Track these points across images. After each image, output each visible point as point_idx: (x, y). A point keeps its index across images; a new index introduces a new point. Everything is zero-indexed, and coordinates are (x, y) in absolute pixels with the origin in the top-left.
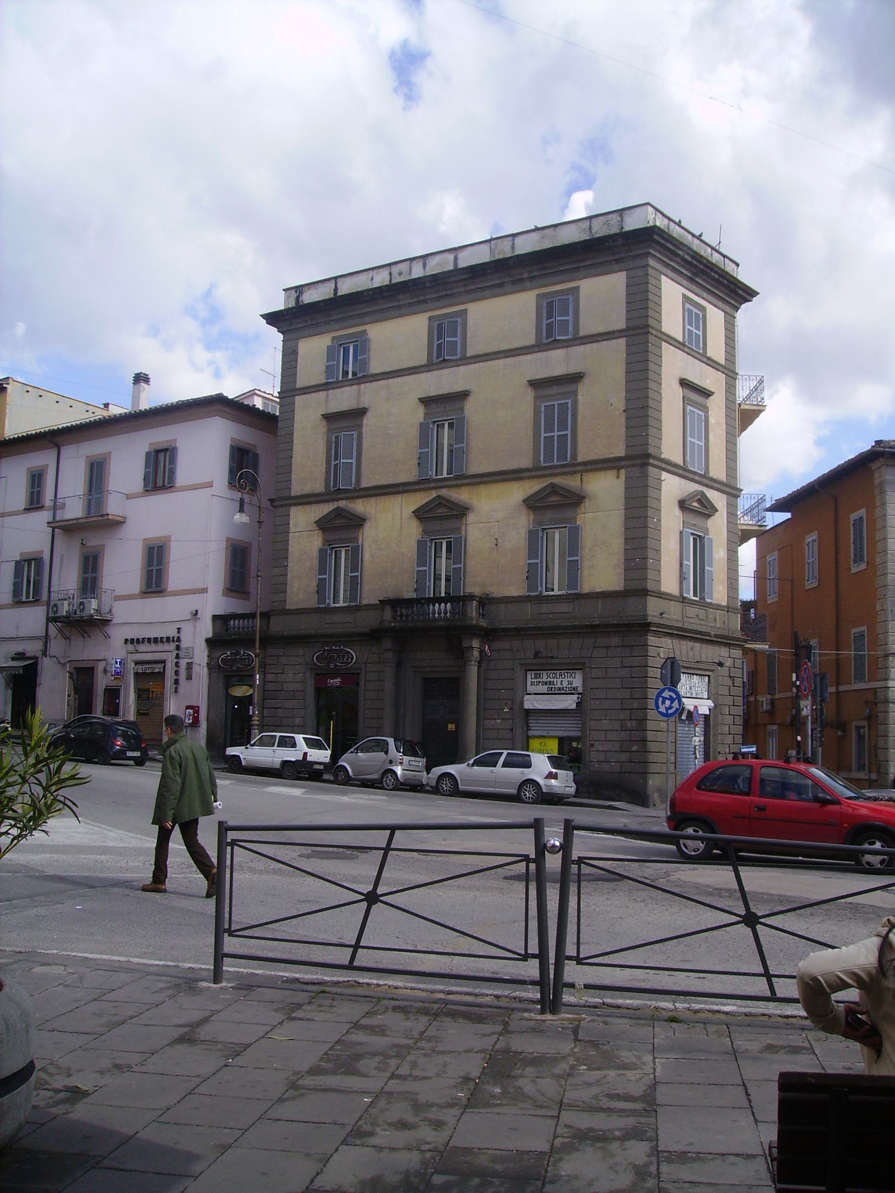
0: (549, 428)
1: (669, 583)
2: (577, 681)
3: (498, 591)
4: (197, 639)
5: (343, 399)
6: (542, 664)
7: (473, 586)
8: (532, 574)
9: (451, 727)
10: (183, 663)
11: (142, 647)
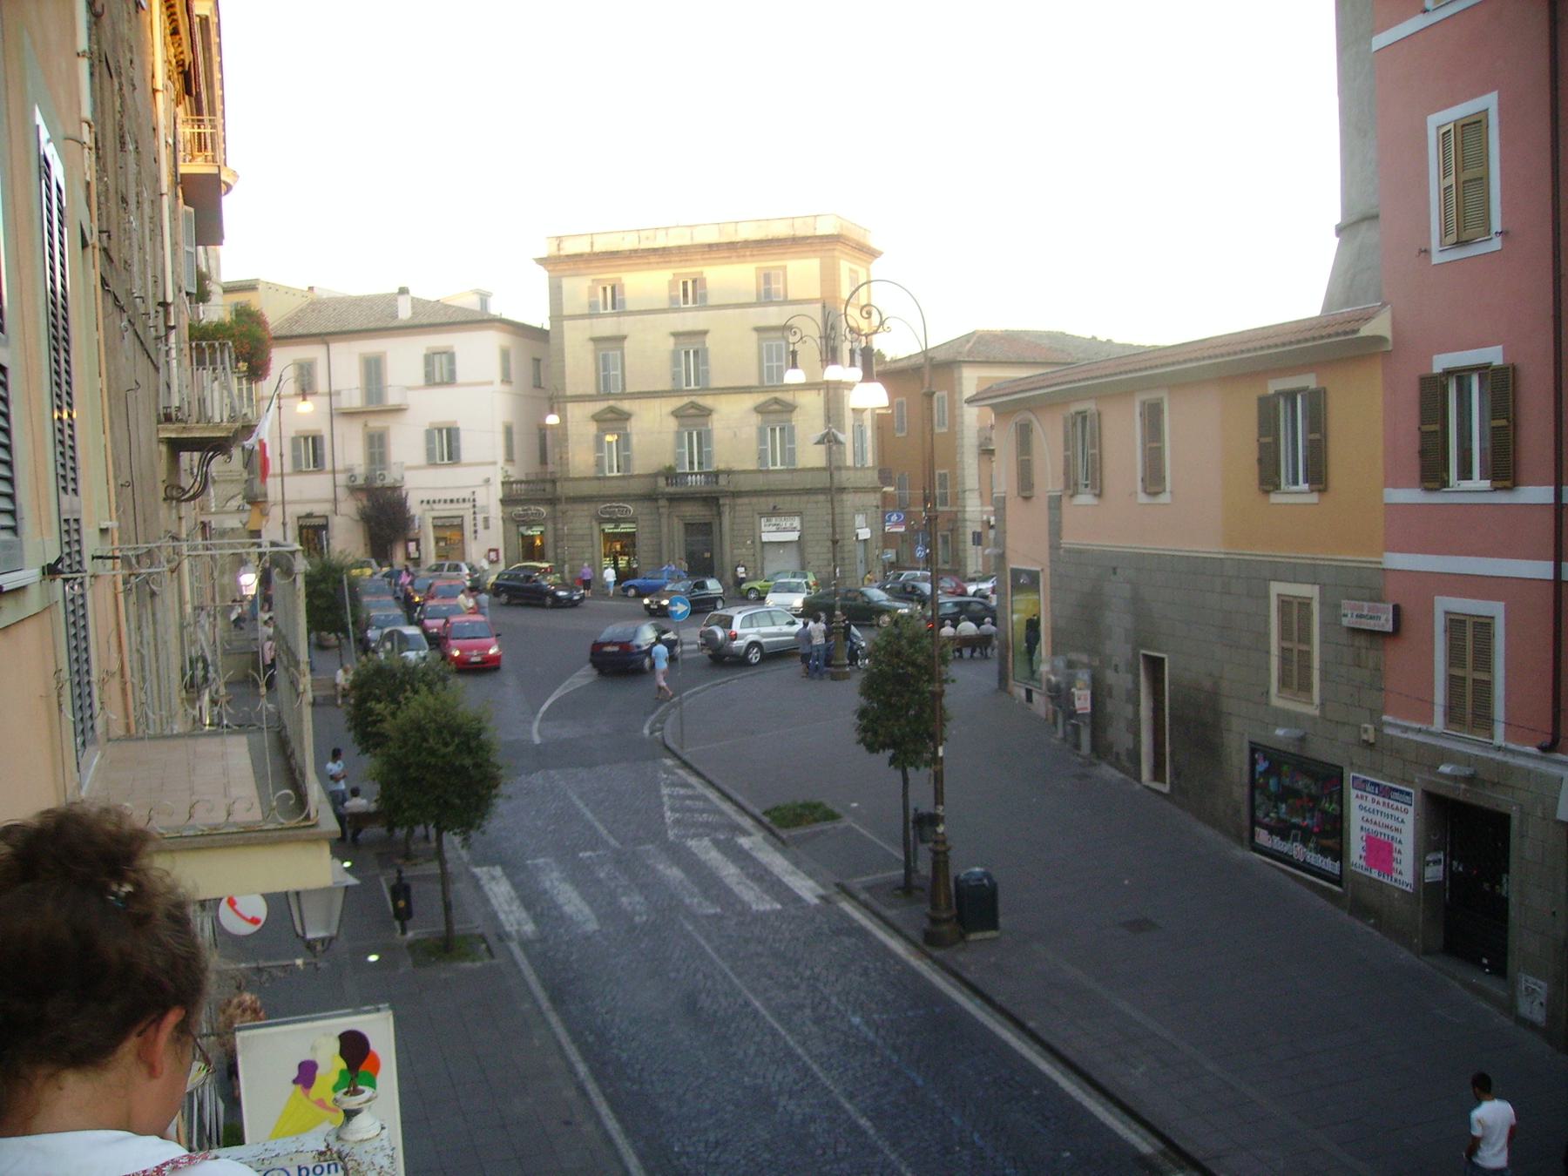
0: (770, 359)
1: (849, 462)
2: (796, 522)
3: (737, 466)
4: (491, 499)
5: (606, 327)
6: (775, 512)
7: (719, 463)
8: (762, 456)
9: (707, 555)
10: (480, 517)
11: (436, 506)
